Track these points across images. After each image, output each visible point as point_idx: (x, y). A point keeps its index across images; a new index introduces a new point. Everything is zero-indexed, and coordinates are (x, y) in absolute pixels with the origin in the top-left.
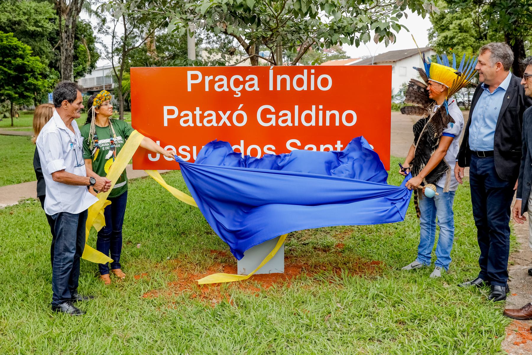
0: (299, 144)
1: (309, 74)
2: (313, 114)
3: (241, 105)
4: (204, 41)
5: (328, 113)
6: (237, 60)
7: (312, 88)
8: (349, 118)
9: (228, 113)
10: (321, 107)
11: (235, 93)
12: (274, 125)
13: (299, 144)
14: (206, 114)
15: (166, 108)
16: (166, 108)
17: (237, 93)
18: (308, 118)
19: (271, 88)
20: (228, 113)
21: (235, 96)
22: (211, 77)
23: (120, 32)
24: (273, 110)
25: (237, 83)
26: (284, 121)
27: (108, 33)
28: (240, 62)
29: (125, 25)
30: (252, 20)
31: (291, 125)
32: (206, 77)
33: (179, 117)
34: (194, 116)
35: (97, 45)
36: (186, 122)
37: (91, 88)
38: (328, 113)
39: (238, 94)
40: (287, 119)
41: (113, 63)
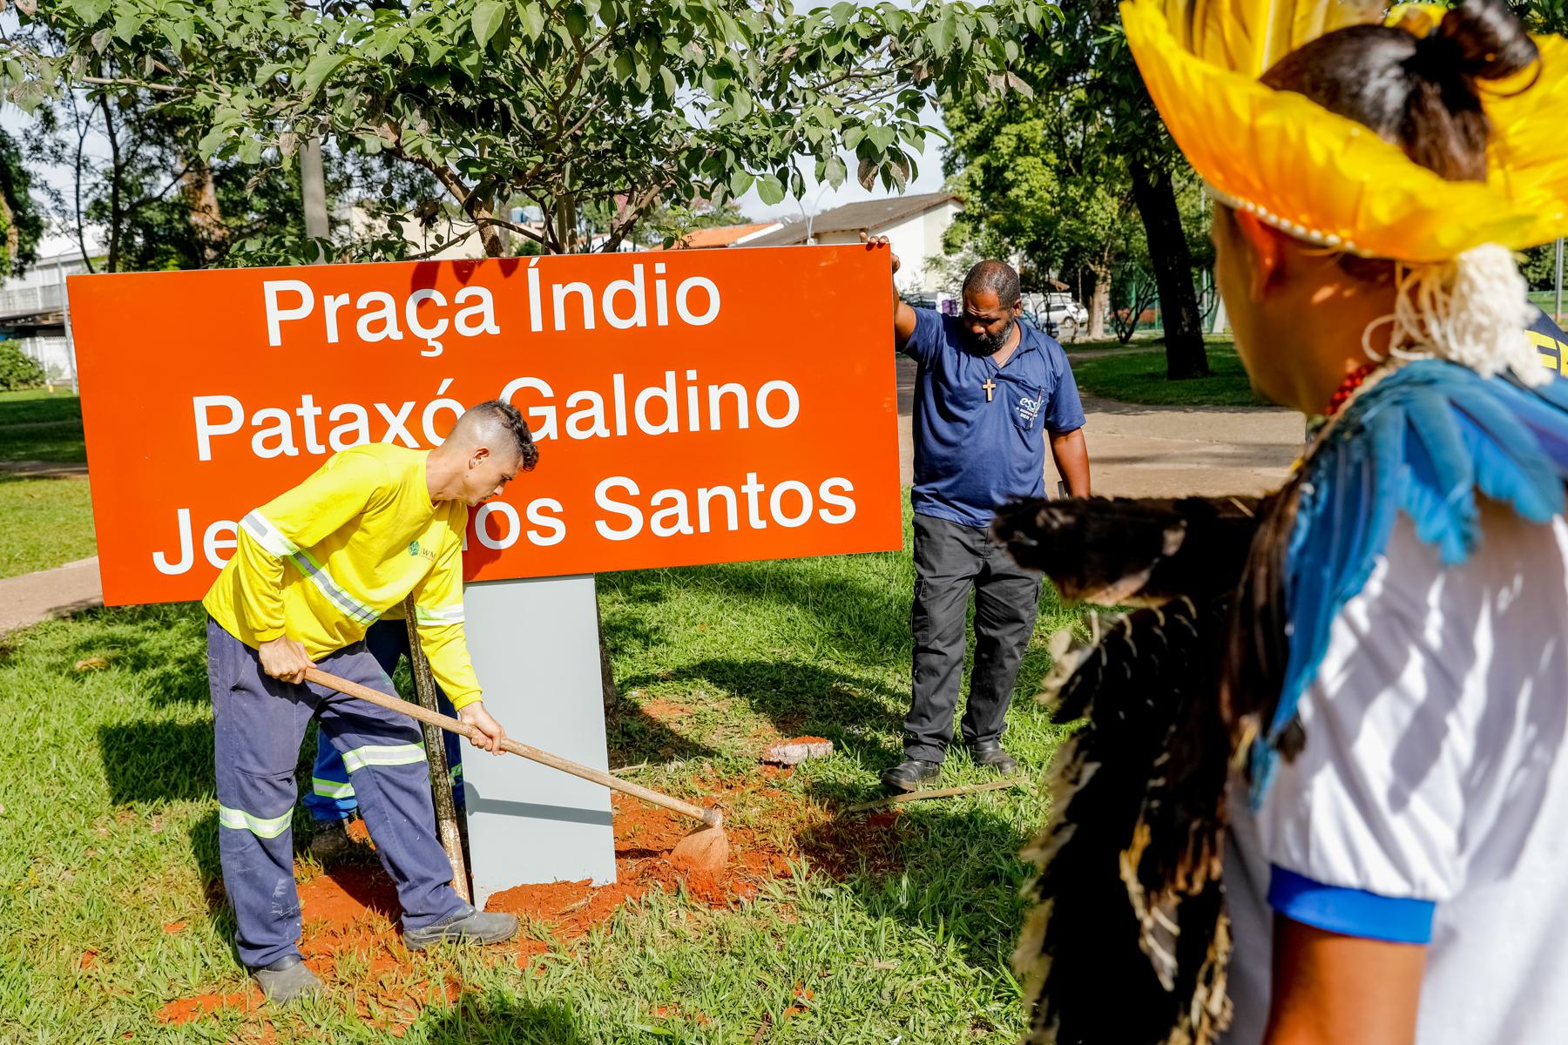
0: (633, 489)
1: (650, 278)
2: (670, 396)
3: (446, 383)
4: (356, 181)
5: (715, 393)
6: (439, 238)
7: (663, 320)
8: (778, 404)
9: (408, 407)
10: (692, 375)
11: (423, 344)
12: (554, 436)
13: (633, 489)
14: (335, 415)
15: (201, 404)
16: (201, 404)
17: (430, 343)
18: (656, 411)
19: (537, 325)
20: (408, 407)
21: (424, 353)
22: (344, 299)
23: (99, 149)
24: (547, 392)
25: (428, 314)
26: (584, 424)
27: (59, 159)
28: (450, 244)
29: (112, 136)
30: (485, 115)
31: (605, 433)
32: (328, 299)
33: (248, 430)
34: (298, 425)
35: (35, 195)
36: (272, 442)
37: (26, 317)
38: (715, 393)
39: (433, 349)
40: (592, 415)
41: (82, 246)
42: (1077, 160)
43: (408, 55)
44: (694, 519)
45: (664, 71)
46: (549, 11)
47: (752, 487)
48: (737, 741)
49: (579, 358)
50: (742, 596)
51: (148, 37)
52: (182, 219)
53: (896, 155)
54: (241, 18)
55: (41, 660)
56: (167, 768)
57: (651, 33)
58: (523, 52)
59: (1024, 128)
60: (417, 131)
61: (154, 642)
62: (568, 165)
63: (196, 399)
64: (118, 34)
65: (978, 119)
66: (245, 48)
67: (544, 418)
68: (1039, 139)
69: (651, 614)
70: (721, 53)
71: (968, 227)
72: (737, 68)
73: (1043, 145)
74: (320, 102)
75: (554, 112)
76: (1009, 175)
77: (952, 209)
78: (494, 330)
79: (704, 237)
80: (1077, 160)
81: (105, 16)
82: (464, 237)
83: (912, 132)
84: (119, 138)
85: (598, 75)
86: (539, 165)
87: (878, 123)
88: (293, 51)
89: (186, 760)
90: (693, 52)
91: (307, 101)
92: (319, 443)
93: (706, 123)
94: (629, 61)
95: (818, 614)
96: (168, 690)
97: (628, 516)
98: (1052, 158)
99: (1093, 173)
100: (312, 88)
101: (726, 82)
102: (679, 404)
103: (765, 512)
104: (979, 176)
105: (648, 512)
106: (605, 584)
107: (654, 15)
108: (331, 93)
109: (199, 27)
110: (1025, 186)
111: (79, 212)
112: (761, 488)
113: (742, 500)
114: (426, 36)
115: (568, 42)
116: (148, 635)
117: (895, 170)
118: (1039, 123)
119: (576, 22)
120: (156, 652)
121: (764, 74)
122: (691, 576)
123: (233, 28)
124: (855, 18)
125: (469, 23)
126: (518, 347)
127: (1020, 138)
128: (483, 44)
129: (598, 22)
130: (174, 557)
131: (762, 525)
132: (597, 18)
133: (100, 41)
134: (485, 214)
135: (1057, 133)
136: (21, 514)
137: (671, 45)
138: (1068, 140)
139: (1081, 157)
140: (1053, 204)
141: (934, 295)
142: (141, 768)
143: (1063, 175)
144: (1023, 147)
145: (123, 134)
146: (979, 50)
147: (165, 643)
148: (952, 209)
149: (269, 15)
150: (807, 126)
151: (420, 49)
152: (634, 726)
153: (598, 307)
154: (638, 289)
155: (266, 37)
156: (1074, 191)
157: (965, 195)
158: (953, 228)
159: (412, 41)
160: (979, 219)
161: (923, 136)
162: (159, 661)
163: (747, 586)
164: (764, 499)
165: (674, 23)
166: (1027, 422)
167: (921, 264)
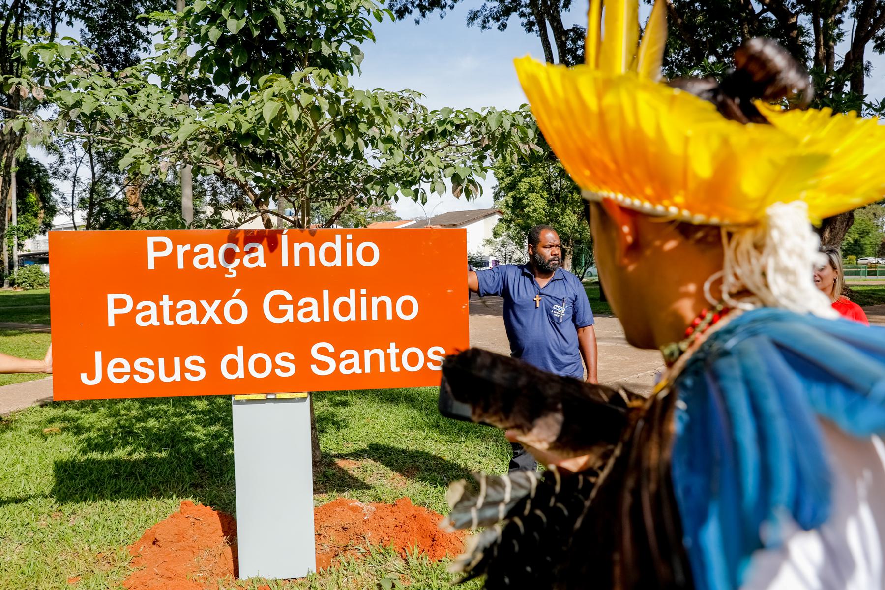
0: (331, 349)
1: (344, 242)
3: (237, 291)
5: (375, 301)
7: (350, 263)
9: (217, 303)
12: (291, 320)
13: (331, 349)
14: (179, 305)
15: (111, 298)
16: (111, 298)
17: (230, 271)
18: (345, 309)
19: (285, 263)
20: (217, 303)
21: (227, 276)
22: (188, 247)
23: (85, 174)
24: (289, 297)
27: (66, 178)
28: (245, 222)
29: (93, 168)
32: (180, 247)
33: (134, 312)
34: (160, 310)
38: (375, 301)
39: (231, 273)
42: (557, 196)
43: (232, 127)
44: (362, 366)
45: (360, 140)
46: (302, 109)
47: (393, 350)
48: (383, 482)
49: (306, 281)
50: (389, 405)
51: (99, 113)
52: (124, 209)
53: (472, 182)
54: (146, 106)
55: (25, 428)
56: (83, 488)
57: (353, 121)
58: (288, 129)
59: (533, 180)
60: (231, 165)
61: (88, 419)
62: (308, 185)
63: (109, 295)
64: (83, 111)
65: (510, 175)
66: (148, 121)
67: (286, 311)
68: (539, 185)
69: (341, 413)
70: (388, 133)
71: (505, 225)
72: (396, 139)
73: (541, 188)
74: (184, 148)
75: (302, 159)
76: (525, 202)
77: (497, 217)
78: (263, 265)
79: (375, 226)
80: (557, 196)
81: (77, 102)
82: (252, 219)
83: (479, 169)
84: (96, 169)
85: (325, 141)
86: (293, 184)
87: (463, 166)
88: (172, 123)
89: (93, 484)
90: (374, 131)
91: (176, 146)
92: (170, 319)
93: (378, 165)
94: (342, 135)
95: (427, 415)
96: (89, 445)
97: (328, 363)
98: (545, 194)
99: (565, 202)
100: (181, 141)
101: (390, 145)
102: (357, 306)
103: (399, 363)
104: (511, 201)
105: (338, 361)
106: (316, 396)
107: (355, 112)
108: (190, 143)
109: (125, 109)
110: (532, 207)
111: (73, 204)
112: (398, 350)
113: (388, 357)
114: (241, 118)
115: (311, 125)
116: (83, 416)
117: (471, 187)
118: (540, 178)
119: (316, 114)
120: (87, 425)
121: (408, 143)
122: (362, 393)
123: (143, 111)
124: (453, 115)
125: (261, 113)
126: (275, 275)
127: (530, 183)
128: (268, 122)
129: (328, 116)
130: (91, 377)
131: (397, 370)
132: (327, 113)
133: (74, 114)
134: (264, 207)
135: (548, 183)
136: (28, 351)
137: (363, 128)
138: (553, 187)
139: (559, 195)
140: (546, 216)
141: (488, 258)
142: (69, 488)
143: (551, 203)
144: (532, 189)
145: (98, 167)
146: (514, 131)
147: (91, 420)
148: (497, 217)
149: (161, 105)
150: (426, 166)
151: (238, 125)
152: (330, 472)
153: (317, 255)
154: (338, 247)
155: (159, 116)
156: (557, 210)
157: (503, 210)
158: (498, 226)
159: (234, 120)
160: (510, 221)
161: (486, 171)
162: (89, 430)
163: (390, 397)
164: (399, 356)
165: (365, 116)
166: (559, 318)
167: (482, 242)
